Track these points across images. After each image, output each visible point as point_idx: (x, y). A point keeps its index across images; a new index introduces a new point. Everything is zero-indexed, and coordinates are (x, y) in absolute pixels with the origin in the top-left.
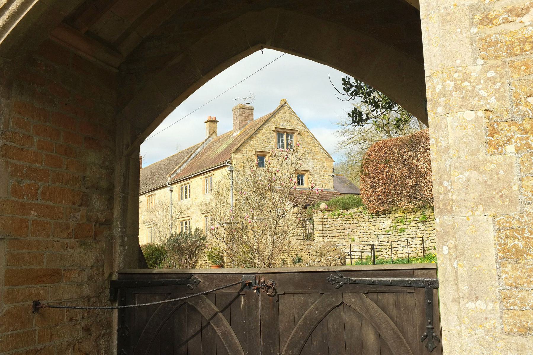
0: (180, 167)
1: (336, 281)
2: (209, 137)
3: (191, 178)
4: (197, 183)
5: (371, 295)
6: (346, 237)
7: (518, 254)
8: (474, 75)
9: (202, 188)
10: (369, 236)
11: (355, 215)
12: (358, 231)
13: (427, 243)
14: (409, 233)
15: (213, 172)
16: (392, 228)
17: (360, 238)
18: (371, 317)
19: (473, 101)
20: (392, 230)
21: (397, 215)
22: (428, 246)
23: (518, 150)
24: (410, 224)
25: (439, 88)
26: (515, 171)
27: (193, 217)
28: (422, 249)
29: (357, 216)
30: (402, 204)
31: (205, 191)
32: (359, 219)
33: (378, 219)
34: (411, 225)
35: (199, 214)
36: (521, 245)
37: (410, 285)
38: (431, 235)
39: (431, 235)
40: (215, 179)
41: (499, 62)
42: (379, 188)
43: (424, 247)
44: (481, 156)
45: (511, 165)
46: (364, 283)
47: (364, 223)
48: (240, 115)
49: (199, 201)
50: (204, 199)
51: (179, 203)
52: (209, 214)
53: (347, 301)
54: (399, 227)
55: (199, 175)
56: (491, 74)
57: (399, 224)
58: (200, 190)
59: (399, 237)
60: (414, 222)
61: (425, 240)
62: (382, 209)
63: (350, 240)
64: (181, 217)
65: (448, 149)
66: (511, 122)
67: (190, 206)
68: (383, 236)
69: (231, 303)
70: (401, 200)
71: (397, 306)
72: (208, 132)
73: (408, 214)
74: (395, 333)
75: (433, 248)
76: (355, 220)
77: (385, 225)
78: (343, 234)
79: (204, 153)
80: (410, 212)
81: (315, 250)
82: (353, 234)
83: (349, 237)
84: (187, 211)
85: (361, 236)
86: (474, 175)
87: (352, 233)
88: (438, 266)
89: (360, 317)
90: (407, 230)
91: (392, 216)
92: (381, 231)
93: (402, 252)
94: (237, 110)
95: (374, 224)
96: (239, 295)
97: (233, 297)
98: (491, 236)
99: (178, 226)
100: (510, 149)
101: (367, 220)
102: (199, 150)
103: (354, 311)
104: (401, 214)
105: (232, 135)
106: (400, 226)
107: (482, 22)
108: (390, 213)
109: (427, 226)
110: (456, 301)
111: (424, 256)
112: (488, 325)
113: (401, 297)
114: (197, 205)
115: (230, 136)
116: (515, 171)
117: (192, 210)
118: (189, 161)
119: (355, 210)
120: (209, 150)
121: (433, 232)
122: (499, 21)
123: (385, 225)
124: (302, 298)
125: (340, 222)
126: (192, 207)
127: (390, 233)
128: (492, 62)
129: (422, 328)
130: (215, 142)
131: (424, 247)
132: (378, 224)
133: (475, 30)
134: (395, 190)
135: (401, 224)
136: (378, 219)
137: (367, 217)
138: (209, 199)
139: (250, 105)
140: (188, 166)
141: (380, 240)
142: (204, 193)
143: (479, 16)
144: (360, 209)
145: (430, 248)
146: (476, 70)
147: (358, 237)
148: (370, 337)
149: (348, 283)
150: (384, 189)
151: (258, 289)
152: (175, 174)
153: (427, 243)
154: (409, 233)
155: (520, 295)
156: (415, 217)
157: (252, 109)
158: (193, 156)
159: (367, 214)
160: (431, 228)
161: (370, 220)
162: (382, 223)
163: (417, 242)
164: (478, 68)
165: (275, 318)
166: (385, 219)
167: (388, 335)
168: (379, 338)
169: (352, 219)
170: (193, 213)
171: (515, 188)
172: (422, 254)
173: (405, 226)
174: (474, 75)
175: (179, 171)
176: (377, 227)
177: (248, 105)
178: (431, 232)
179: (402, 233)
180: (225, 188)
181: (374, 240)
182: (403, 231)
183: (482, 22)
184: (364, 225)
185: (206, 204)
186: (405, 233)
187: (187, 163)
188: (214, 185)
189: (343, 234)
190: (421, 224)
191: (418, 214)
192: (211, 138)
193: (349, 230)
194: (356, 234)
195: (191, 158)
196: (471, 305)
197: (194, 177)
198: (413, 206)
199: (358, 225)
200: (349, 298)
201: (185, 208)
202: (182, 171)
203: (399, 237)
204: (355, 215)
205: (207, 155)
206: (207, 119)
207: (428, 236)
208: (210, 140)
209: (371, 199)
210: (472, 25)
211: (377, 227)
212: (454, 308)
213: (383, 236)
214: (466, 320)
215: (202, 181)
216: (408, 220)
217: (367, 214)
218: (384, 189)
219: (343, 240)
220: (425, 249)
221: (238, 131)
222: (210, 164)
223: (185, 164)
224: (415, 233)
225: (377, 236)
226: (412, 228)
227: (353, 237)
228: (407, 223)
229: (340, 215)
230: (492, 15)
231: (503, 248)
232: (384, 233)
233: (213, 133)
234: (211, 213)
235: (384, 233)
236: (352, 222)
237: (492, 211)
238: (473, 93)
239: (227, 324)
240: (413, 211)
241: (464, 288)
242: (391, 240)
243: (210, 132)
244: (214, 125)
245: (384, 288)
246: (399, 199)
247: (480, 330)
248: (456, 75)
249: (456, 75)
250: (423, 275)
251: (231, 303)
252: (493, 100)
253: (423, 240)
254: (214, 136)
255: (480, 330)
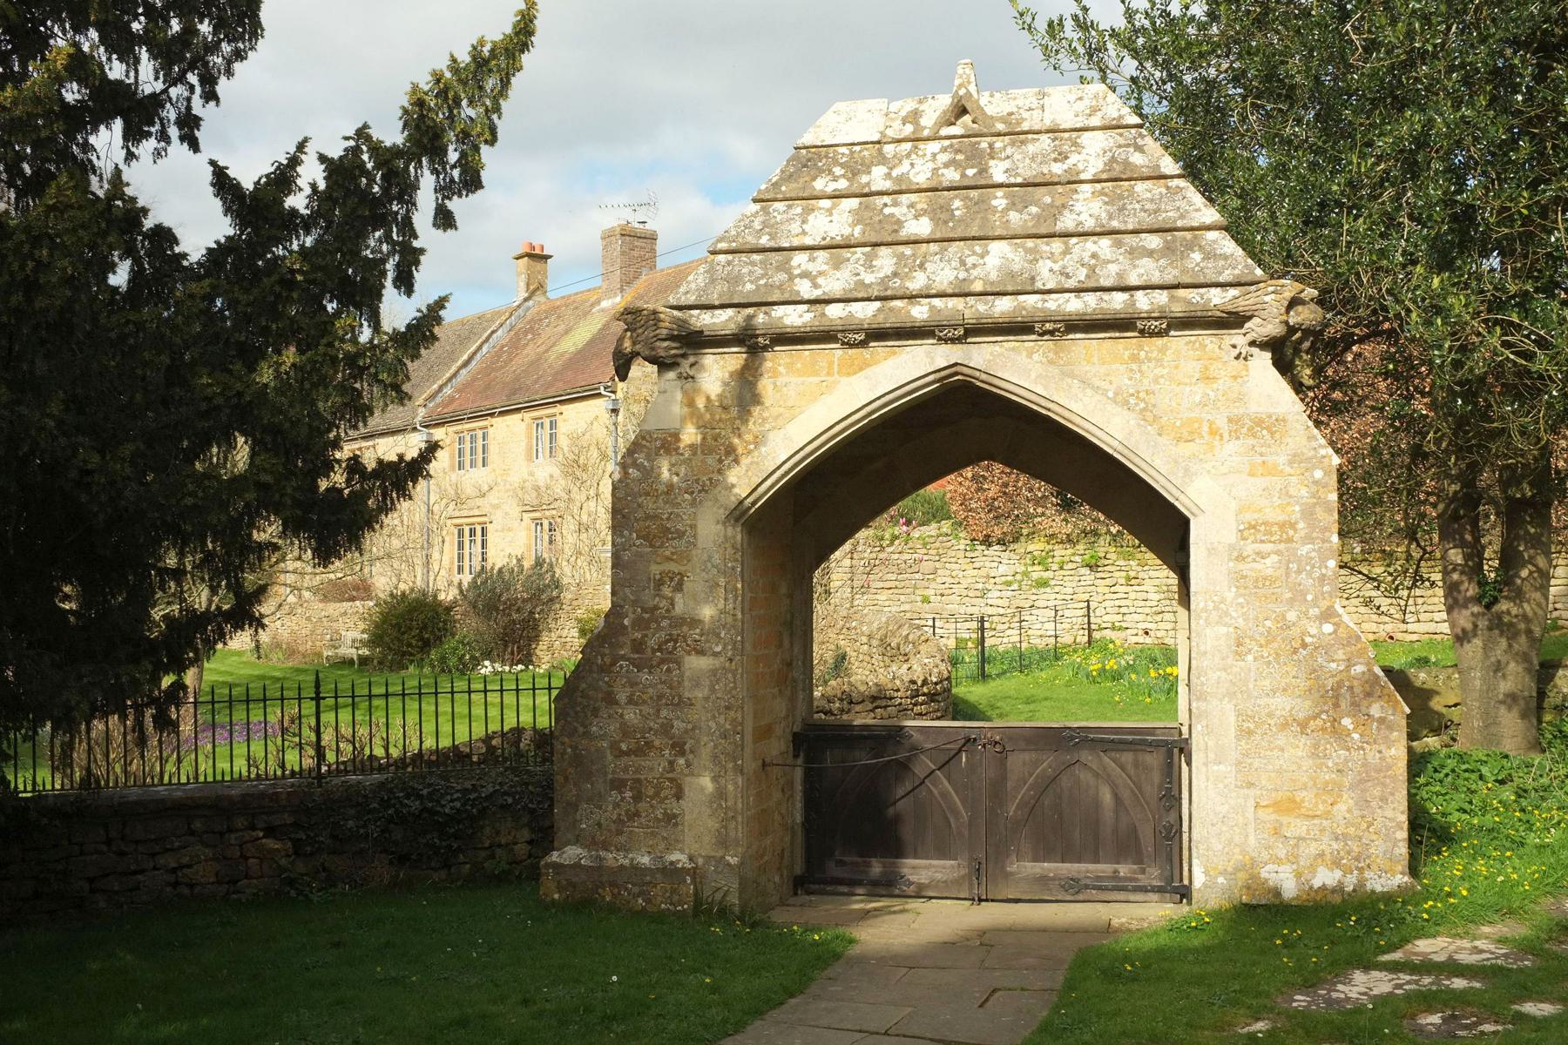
0: (450, 379)
1: (1072, 738)
2: (526, 300)
3: (492, 415)
4: (509, 432)
5: (1109, 754)
6: (908, 591)
7: (1250, 733)
8: (1229, 600)
9: (524, 444)
10: (965, 593)
11: (932, 540)
12: (939, 580)
13: (1098, 614)
14: (1057, 589)
15: (560, 408)
16: (1018, 577)
17: (942, 595)
18: (1109, 776)
19: (1227, 620)
20: (1020, 582)
21: (1031, 548)
22: (1099, 621)
23: (1255, 659)
24: (1061, 568)
25: (1202, 605)
26: (1252, 674)
27: (497, 517)
28: (1086, 626)
29: (937, 544)
30: (1046, 522)
31: (532, 454)
32: (941, 551)
33: (986, 552)
34: (1062, 572)
35: (515, 510)
36: (1252, 726)
37: (1150, 744)
38: (1106, 597)
39: (1106, 597)
40: (563, 428)
41: (1247, 592)
42: (992, 482)
43: (1089, 623)
44: (1230, 661)
45: (1250, 670)
46: (1102, 741)
47: (953, 560)
48: (623, 253)
49: (515, 479)
50: (532, 474)
51: (454, 477)
52: (547, 513)
53: (1083, 759)
54: (1035, 576)
55: (518, 410)
56: (1241, 600)
57: (1036, 568)
58: (519, 447)
59: (1035, 597)
60: (1070, 566)
61: (1092, 608)
62: (998, 532)
63: (919, 598)
64: (457, 514)
65: (1206, 653)
66: (1252, 638)
67: (486, 488)
68: (999, 594)
69: (950, 759)
70: (1043, 514)
71: (1136, 765)
72: (522, 285)
73: (1056, 547)
74: (1132, 791)
75: (1110, 625)
76: (931, 552)
77: (1002, 569)
78: (903, 584)
79: (515, 344)
80: (1062, 542)
81: (867, 633)
82: (926, 584)
83: (917, 592)
84: (479, 502)
85: (946, 592)
86: (1223, 675)
87: (925, 583)
88: (1193, 735)
89: (1097, 775)
90: (1052, 583)
91: (1020, 547)
92: (992, 581)
93: (1039, 633)
94: (613, 238)
95: (977, 565)
96: (960, 751)
97: (953, 752)
98: (1233, 719)
99: (447, 539)
100: (1250, 658)
101: (961, 554)
102: (499, 333)
103: (1090, 769)
104: (1041, 546)
105: (598, 302)
106: (1037, 573)
107: (1237, 559)
108: (1016, 540)
109: (1099, 575)
110: (1206, 764)
111: (1089, 642)
112: (1226, 781)
113: (1141, 756)
114: (508, 487)
115: (593, 305)
116: (1252, 674)
117: (492, 498)
118: (474, 363)
119: (931, 529)
120: (532, 340)
121: (1113, 589)
122: (1250, 559)
123: (1002, 569)
124: (1034, 755)
125: (896, 556)
126: (492, 492)
127: (1015, 586)
128: (1242, 591)
129: (1160, 788)
130: (548, 313)
131: (1089, 623)
132: (987, 564)
133: (1231, 564)
134: (1031, 490)
135: (1040, 568)
136: (986, 552)
137: (962, 547)
138: (546, 475)
139: (647, 226)
140: (474, 380)
141: (990, 602)
142: (529, 459)
143: (1235, 554)
144: (946, 526)
145: (1104, 625)
146: (1230, 595)
147: (938, 592)
148: (1107, 797)
149: (1085, 740)
150: (1006, 485)
151: (984, 746)
152: (438, 399)
153: (1098, 614)
154: (1057, 589)
155: (1249, 761)
156: (1074, 554)
157: (652, 238)
158: (485, 349)
159: (962, 541)
160: (1108, 582)
161: (968, 554)
162: (996, 564)
163: (1075, 614)
164: (1233, 594)
165: (1002, 778)
166: (1003, 554)
167: (1125, 795)
168: (1117, 798)
169: (925, 551)
170: (497, 507)
171: (1251, 686)
172: (1086, 639)
173: (1049, 574)
174: (1229, 600)
175: (448, 391)
176: (983, 572)
177: (641, 226)
178: (1107, 590)
179: (1042, 590)
180: (595, 453)
181: (975, 601)
182: (1043, 584)
183: (1237, 559)
184: (953, 566)
185: (537, 489)
186: (1048, 590)
187: (469, 367)
188: (563, 441)
189: (903, 584)
190: (1086, 571)
191: (1081, 547)
192: (531, 303)
193: (917, 576)
194: (933, 585)
195: (478, 356)
196: (1215, 768)
197: (502, 413)
198: (1069, 529)
199: (938, 565)
200: (1086, 756)
201: (470, 491)
202: (460, 391)
203: (1035, 597)
204: (932, 540)
205: (530, 352)
206: (521, 251)
207: (1100, 598)
208: (529, 309)
209: (974, 506)
210: (1230, 560)
211: (983, 572)
212: (1204, 769)
213: (999, 594)
214: (1212, 779)
215: (523, 425)
216: (1057, 559)
217: (962, 541)
218: (1006, 485)
219: (902, 598)
220: (1093, 627)
221: (615, 296)
222: (550, 385)
223: (464, 372)
224: (1071, 591)
225: (983, 594)
226: (1066, 578)
227: (927, 592)
228: (1055, 567)
229: (895, 538)
230: (1245, 554)
231: (1240, 729)
232: (999, 587)
233: (536, 288)
234: (554, 512)
235: (999, 587)
236: (926, 558)
237: (1234, 702)
238: (1227, 613)
239: (946, 783)
240: (1070, 541)
241: (1211, 756)
242: (1016, 603)
243: (528, 285)
244: (538, 266)
245: (1121, 746)
246: (1040, 510)
247: (1221, 786)
248: (1215, 598)
249: (1215, 598)
250: (1163, 735)
251: (950, 759)
252: (1240, 620)
253: (1088, 607)
254: (538, 298)
255: (1221, 786)
